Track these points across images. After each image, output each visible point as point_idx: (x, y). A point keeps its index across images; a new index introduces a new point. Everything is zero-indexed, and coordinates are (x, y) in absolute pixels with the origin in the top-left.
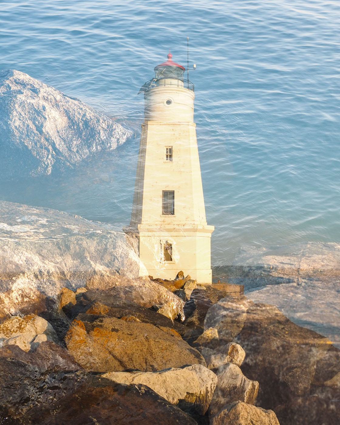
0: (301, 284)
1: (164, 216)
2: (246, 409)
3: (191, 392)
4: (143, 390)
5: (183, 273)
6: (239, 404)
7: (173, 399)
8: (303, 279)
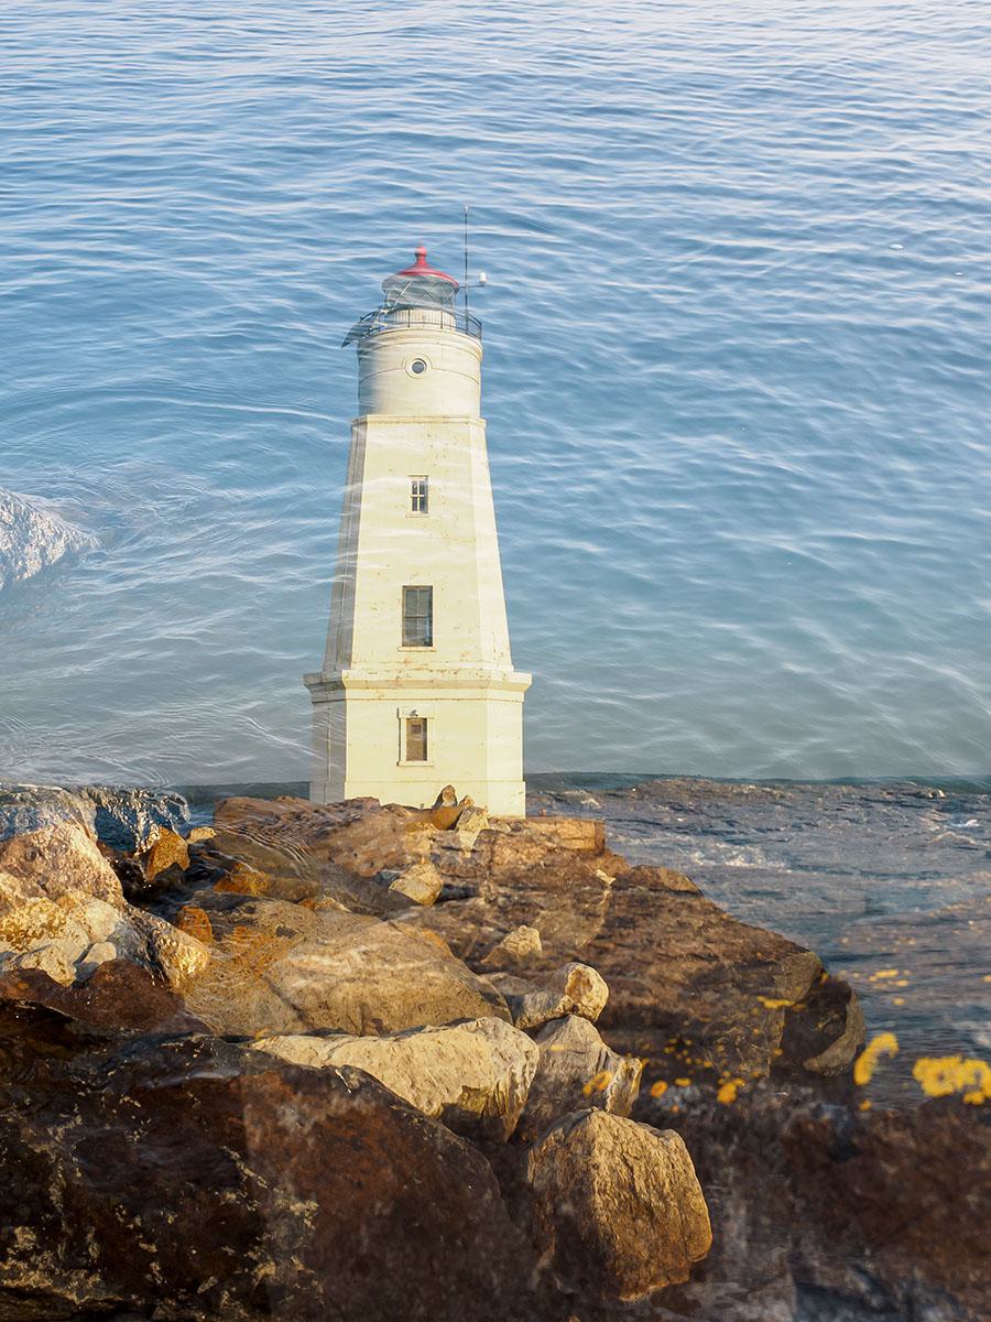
0: (496, 899)
1: (408, 648)
2: (610, 1127)
3: (473, 1087)
4: (354, 1080)
5: (454, 791)
6: (593, 1116)
7: (430, 1102)
8: (501, 885)
